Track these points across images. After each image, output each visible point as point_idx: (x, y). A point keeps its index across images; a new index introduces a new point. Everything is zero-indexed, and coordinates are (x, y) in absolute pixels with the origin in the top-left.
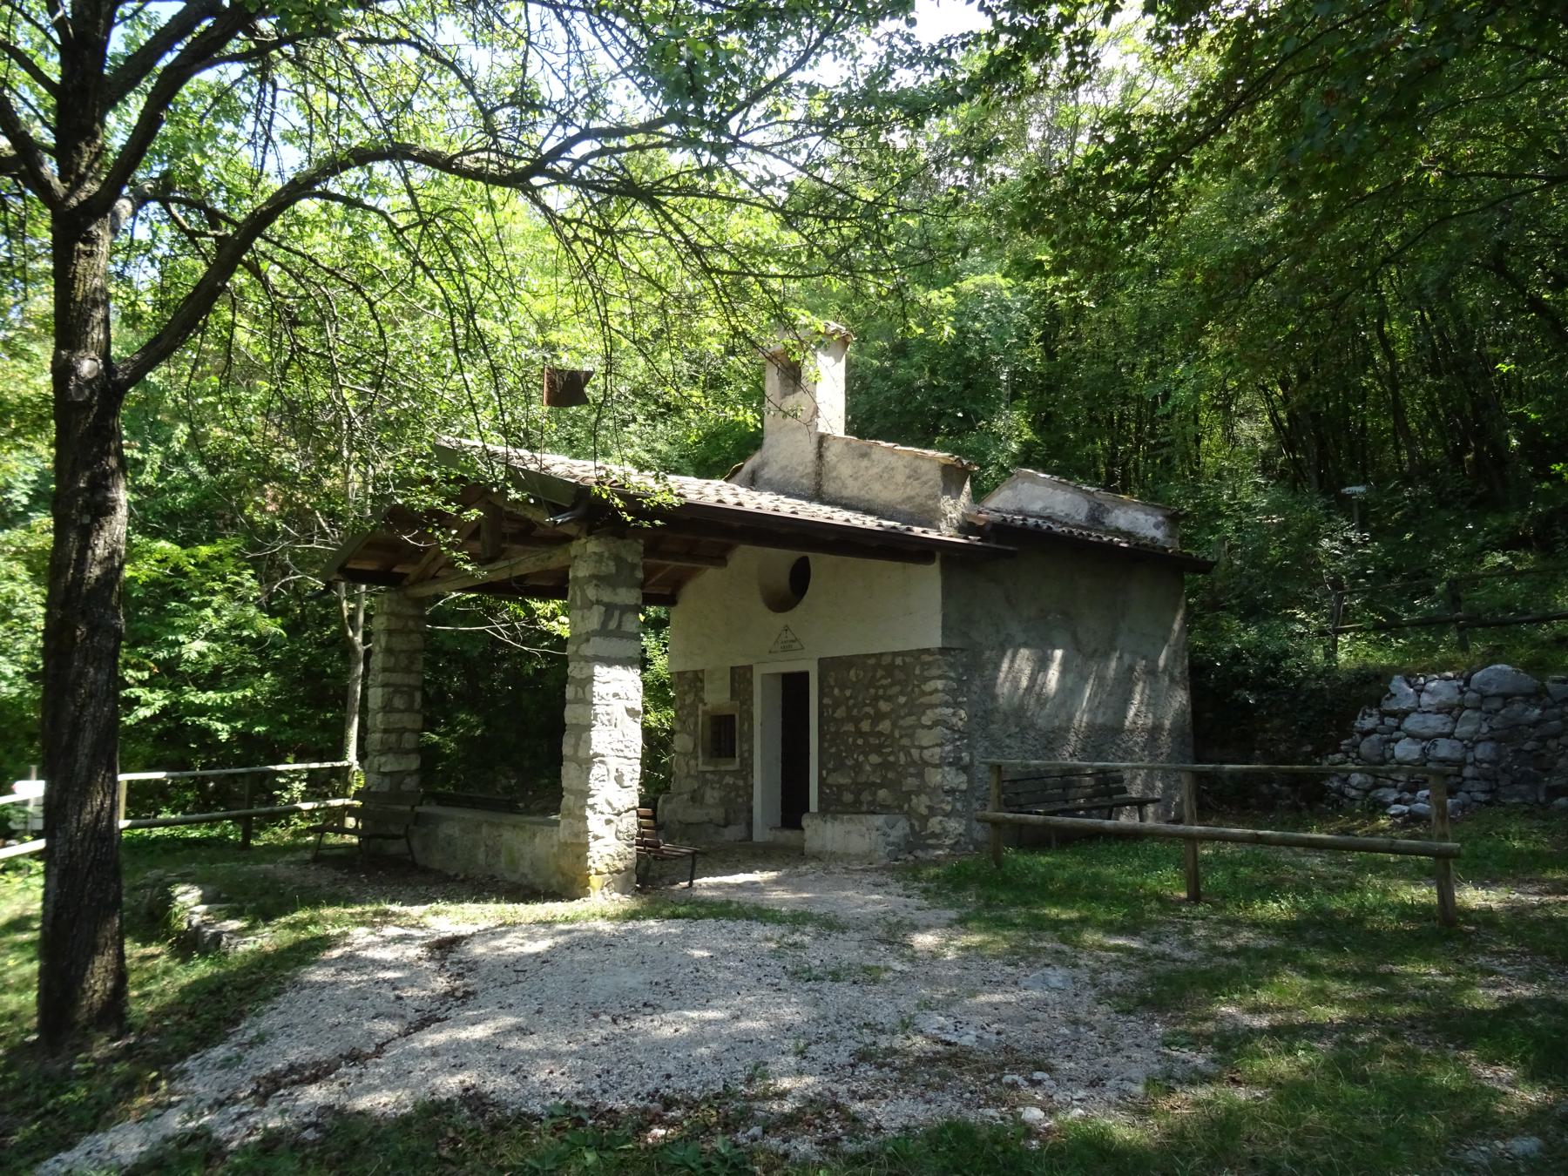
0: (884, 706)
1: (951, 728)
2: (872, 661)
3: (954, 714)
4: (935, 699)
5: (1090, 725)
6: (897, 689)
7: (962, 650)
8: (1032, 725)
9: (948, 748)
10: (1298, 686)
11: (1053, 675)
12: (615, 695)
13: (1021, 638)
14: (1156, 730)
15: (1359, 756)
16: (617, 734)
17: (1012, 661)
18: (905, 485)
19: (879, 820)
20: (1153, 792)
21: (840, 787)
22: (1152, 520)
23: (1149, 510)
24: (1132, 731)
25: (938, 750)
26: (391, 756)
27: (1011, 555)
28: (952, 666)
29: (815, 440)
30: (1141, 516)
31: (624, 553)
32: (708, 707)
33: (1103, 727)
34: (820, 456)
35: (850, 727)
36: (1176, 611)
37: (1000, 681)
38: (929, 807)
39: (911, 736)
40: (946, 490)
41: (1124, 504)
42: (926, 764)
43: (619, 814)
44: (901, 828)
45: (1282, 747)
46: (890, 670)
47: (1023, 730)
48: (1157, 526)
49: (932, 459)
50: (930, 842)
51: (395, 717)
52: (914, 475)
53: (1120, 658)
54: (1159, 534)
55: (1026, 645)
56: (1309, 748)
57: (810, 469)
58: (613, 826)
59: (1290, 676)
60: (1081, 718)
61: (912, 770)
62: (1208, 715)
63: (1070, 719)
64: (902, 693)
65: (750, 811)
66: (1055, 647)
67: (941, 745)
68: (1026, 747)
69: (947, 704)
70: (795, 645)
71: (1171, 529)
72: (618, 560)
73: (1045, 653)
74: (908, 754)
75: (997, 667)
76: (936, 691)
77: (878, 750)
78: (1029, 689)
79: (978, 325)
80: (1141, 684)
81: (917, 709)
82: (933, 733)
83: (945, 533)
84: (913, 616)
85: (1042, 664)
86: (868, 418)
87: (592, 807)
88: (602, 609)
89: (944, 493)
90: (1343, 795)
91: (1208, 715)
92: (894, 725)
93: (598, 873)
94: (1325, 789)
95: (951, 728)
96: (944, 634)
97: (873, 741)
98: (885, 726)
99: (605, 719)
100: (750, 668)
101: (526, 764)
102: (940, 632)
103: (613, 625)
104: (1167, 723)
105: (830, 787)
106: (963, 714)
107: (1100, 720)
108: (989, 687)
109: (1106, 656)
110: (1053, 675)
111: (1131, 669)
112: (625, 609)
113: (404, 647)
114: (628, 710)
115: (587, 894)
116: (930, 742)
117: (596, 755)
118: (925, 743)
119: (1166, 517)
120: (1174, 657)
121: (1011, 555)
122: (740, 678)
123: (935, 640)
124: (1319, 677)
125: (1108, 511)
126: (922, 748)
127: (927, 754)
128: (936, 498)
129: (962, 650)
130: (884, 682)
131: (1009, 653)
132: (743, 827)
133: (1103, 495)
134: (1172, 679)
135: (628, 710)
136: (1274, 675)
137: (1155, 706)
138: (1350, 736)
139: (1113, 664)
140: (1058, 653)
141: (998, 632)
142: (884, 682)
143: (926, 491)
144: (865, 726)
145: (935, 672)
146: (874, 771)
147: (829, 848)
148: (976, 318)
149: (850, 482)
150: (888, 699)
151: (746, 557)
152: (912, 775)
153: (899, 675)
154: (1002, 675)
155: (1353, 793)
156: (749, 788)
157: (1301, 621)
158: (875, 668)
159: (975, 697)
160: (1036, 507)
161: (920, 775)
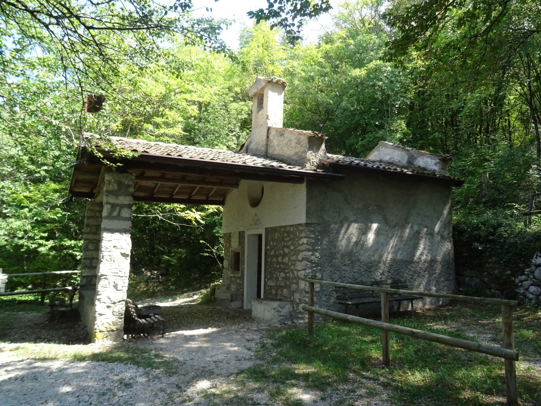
0: (286, 250)
1: (311, 262)
2: (283, 229)
3: (312, 255)
4: (303, 248)
5: (393, 260)
6: (290, 242)
7: (318, 224)
8: (358, 260)
9: (308, 271)
10: (505, 241)
11: (371, 237)
12: (114, 247)
13: (352, 218)
14: (433, 262)
15: (534, 277)
16: (115, 265)
17: (347, 229)
18: (295, 147)
19: (275, 304)
20: (426, 291)
21: (271, 286)
22: (434, 161)
23: (433, 157)
24: (418, 263)
25: (303, 272)
26: (87, 269)
27: (342, 178)
28: (313, 232)
29: (266, 130)
30: (429, 160)
31: (123, 180)
32: (233, 249)
33: (402, 261)
34: (268, 137)
35: (275, 260)
36: (445, 204)
37: (340, 239)
38: (299, 299)
39: (294, 265)
40: (310, 148)
41: (422, 155)
42: (300, 278)
43: (114, 303)
44: (287, 308)
45: (496, 272)
46: (289, 233)
47: (353, 262)
48: (436, 164)
49: (304, 134)
50: (300, 316)
51: (90, 253)
52: (298, 143)
53: (412, 227)
54: (436, 168)
55: (356, 221)
56: (509, 272)
57: (264, 143)
58: (111, 309)
59: (501, 236)
60: (388, 257)
61: (294, 281)
62: (465, 254)
63: (381, 257)
64: (292, 244)
65: (243, 294)
66: (372, 223)
67: (305, 270)
68: (355, 270)
69: (308, 250)
70: (258, 222)
71: (443, 166)
72: (119, 183)
73: (367, 225)
74: (293, 274)
75: (338, 233)
76: (303, 244)
77: (283, 270)
78: (357, 243)
79: (381, 83)
80: (424, 240)
81: (297, 252)
82: (303, 263)
83: (309, 168)
84: (292, 208)
85: (364, 231)
86: (292, 120)
87: (99, 300)
88: (109, 206)
89: (309, 150)
90: (526, 297)
91: (465, 254)
92: (289, 259)
93: (100, 332)
94: (517, 293)
95: (311, 262)
96: (307, 217)
97: (282, 266)
98: (286, 260)
99: (108, 258)
100: (244, 232)
101: (203, 268)
102: (305, 216)
103: (115, 214)
104: (439, 258)
105: (268, 286)
106: (318, 254)
107: (399, 257)
108: (333, 243)
109: (403, 227)
110: (371, 237)
111: (418, 232)
112: (122, 206)
113: (94, 224)
114: (122, 254)
115: (94, 342)
116: (301, 269)
117: (102, 275)
118: (299, 268)
119: (440, 160)
120: (444, 226)
121: (342, 178)
122: (241, 235)
123: (303, 220)
124: (515, 237)
125: (416, 158)
126: (298, 271)
127: (299, 273)
128: (305, 152)
129: (318, 224)
130: (286, 239)
131: (346, 225)
132: (240, 302)
133: (413, 151)
134: (443, 238)
135: (122, 254)
136: (493, 235)
137: (431, 249)
138: (529, 267)
139: (408, 231)
140: (375, 226)
141: (339, 215)
142: (286, 239)
143: (302, 149)
144: (280, 259)
145: (303, 235)
146: (282, 280)
147: (258, 316)
148: (381, 80)
149: (277, 148)
150: (288, 247)
151: (244, 183)
152: (294, 283)
153: (291, 236)
154: (341, 236)
155: (531, 296)
156: (243, 284)
157: (516, 209)
158: (284, 232)
159: (325, 246)
160: (387, 158)
161: (297, 284)
